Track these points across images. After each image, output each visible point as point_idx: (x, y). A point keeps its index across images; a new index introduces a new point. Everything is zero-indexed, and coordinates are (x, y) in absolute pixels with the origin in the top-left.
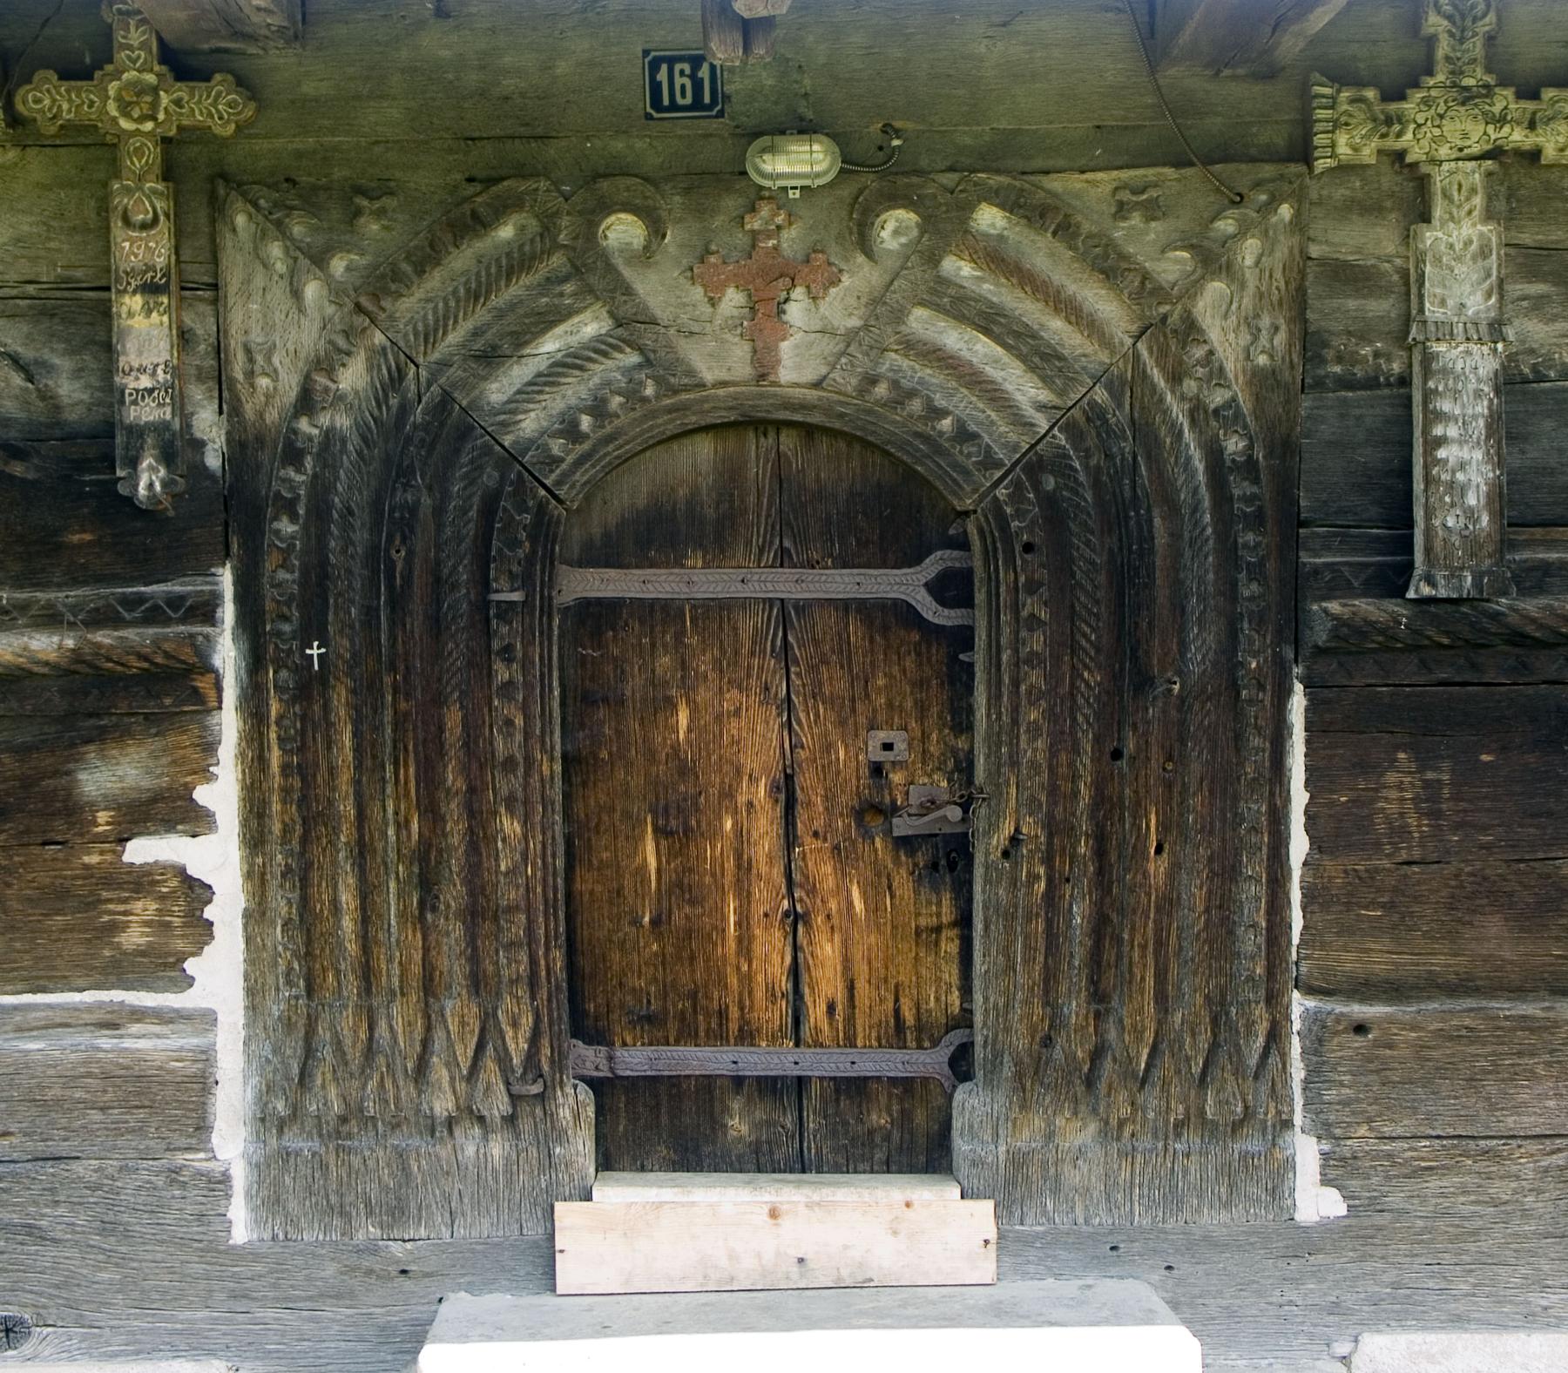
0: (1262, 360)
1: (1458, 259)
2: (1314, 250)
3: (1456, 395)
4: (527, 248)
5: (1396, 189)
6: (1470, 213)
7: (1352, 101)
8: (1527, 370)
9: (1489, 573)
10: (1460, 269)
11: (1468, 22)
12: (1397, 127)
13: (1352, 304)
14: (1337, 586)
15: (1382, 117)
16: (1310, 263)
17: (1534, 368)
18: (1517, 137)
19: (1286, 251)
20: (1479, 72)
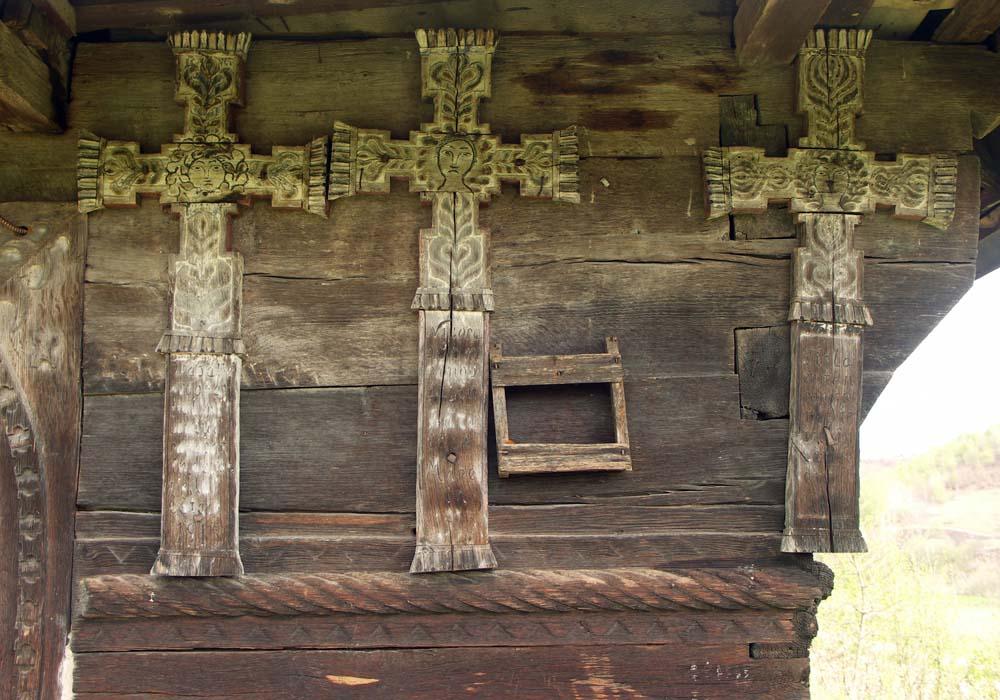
0: (45, 367)
1: (202, 284)
2: (91, 275)
3: (194, 398)
4: (104, 295)
5: (164, 226)
6: (211, 245)
7: (116, 153)
8: (273, 379)
9: (217, 554)
10: (202, 292)
11: (212, 92)
12: (152, 175)
13: (123, 321)
14: (102, 561)
15: (140, 166)
16: (87, 285)
17: (279, 376)
18: (253, 185)
19: (64, 274)
20: (222, 132)
